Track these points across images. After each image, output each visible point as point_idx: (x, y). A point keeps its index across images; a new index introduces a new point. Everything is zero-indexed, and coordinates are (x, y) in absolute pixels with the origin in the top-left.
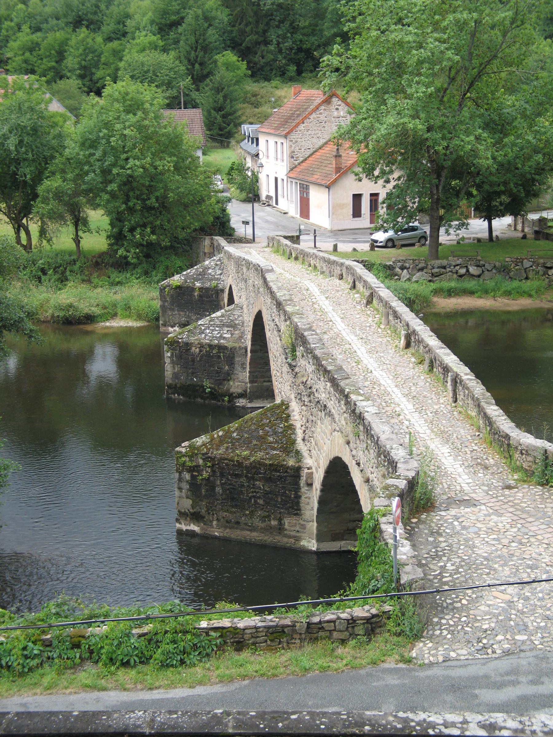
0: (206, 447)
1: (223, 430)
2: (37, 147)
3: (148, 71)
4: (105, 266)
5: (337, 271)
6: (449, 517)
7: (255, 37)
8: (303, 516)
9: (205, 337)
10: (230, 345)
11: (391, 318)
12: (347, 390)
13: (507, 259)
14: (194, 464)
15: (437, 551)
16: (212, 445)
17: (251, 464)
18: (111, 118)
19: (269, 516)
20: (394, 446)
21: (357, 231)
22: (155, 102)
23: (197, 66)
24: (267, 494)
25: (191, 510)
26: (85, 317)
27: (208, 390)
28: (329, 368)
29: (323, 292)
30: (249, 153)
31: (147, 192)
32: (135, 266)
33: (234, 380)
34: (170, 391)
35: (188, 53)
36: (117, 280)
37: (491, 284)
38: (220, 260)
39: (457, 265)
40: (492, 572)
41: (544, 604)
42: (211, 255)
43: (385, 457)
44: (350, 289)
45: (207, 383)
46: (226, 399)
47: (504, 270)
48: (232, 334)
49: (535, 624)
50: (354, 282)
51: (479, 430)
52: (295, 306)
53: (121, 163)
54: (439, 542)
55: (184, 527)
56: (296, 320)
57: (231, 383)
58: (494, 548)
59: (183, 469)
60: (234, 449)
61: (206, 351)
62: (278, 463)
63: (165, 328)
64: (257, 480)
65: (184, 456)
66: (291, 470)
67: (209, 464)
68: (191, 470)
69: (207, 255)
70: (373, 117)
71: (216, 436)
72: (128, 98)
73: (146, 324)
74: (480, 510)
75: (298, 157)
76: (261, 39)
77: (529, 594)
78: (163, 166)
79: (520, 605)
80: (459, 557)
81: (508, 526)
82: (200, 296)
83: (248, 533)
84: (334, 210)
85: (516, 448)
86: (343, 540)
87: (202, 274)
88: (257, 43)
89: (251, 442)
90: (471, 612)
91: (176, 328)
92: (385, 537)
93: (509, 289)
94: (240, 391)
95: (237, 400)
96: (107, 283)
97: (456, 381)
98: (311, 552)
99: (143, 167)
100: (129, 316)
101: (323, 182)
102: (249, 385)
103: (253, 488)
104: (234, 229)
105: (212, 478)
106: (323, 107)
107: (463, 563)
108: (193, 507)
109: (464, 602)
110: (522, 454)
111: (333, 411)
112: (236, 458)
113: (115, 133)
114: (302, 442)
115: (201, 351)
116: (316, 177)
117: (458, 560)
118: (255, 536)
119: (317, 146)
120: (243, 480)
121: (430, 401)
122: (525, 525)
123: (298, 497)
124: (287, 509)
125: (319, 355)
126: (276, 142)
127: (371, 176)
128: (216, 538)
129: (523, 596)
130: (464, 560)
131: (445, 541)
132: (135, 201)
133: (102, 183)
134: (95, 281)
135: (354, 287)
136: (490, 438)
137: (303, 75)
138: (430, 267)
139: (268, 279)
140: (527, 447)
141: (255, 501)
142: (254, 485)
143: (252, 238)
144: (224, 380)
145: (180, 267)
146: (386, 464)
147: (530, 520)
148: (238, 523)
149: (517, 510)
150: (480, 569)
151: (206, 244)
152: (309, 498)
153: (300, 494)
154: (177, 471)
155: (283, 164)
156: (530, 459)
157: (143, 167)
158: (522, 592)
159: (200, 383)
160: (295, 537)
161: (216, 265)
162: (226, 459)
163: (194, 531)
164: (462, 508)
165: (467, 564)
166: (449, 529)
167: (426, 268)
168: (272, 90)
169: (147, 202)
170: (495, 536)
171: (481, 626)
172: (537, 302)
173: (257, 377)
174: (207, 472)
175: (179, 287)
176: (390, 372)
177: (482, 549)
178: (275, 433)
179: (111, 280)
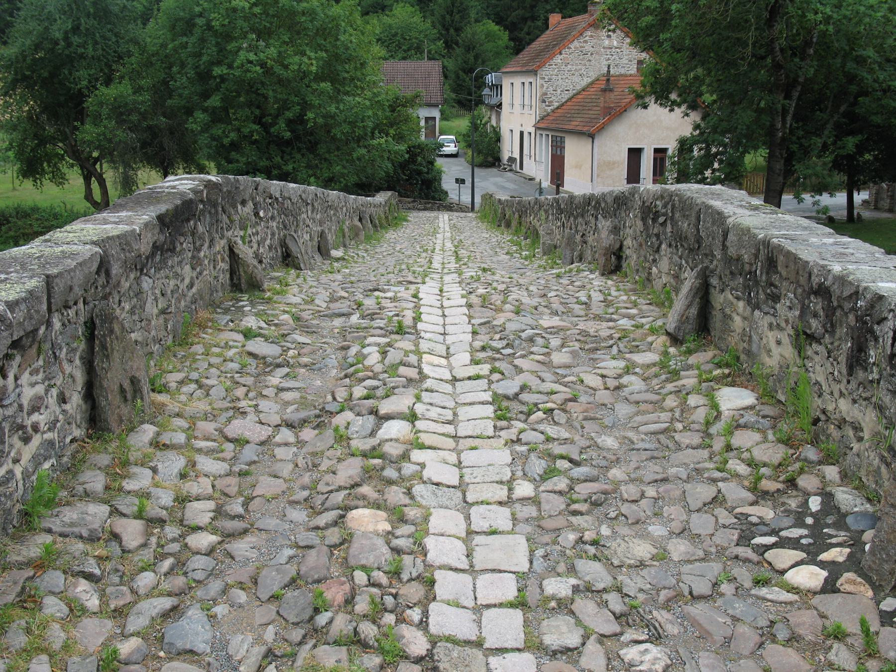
2: (104, 37)
3: (396, 35)
7: (520, 12)
23: (452, 31)
35: (443, 17)
44: (675, 339)
52: (183, 65)
75: (552, 102)
76: (528, 15)
88: (524, 20)
99: (263, 65)
106: (589, 33)
119: (579, 88)
155: (531, 112)
157: (263, 65)
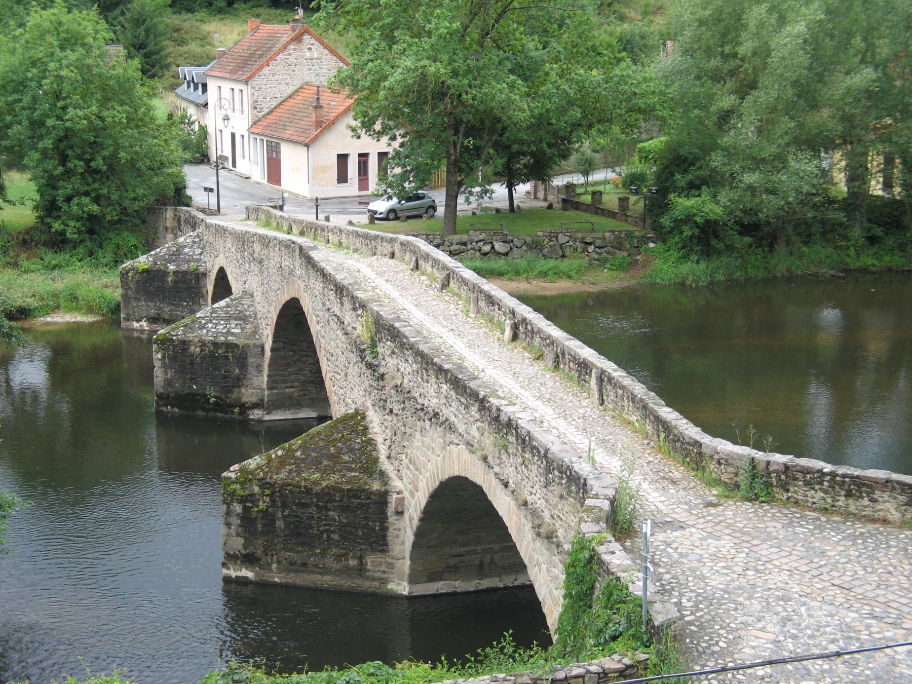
0: (263, 471)
1: (282, 449)
4: (36, 245)
5: (387, 248)
6: (659, 543)
8: (391, 553)
9: (207, 333)
10: (241, 342)
11: (482, 304)
12: (483, 393)
13: (540, 232)
14: (247, 492)
15: (662, 585)
16: (270, 467)
17: (323, 489)
18: (41, 55)
19: (346, 555)
20: (574, 459)
21: (348, 200)
22: (99, 36)
24: (344, 527)
25: (243, 552)
26: (18, 310)
27: (212, 400)
28: (446, 366)
29: (381, 274)
30: (192, 102)
31: (90, 150)
32: (75, 245)
33: (247, 386)
34: (161, 403)
36: (54, 262)
37: (522, 263)
38: (198, 236)
39: (480, 241)
40: (739, 607)
41: (817, 642)
42: (177, 230)
43: (561, 473)
45: (212, 392)
46: (236, 410)
47: (535, 246)
48: (242, 329)
49: (817, 667)
50: (417, 261)
51: (647, 436)
53: (59, 112)
54: (660, 573)
55: (233, 573)
56: (375, 308)
57: (243, 390)
58: (729, 578)
59: (232, 499)
60: (299, 472)
61: (210, 351)
62: (359, 487)
63: (128, 323)
64: (330, 510)
65: (233, 483)
66: (375, 495)
67: (267, 492)
68: (243, 500)
69: (170, 230)
70: (382, 58)
71: (273, 456)
72: (61, 29)
73: (99, 318)
74: (692, 534)
77: (795, 632)
78: (113, 117)
79: (790, 645)
80: (692, 591)
81: (733, 551)
82: (175, 282)
83: (319, 577)
84: (314, 174)
85: (712, 457)
86: (441, 580)
87: (176, 255)
89: (321, 463)
90: (736, 656)
91: (144, 324)
92: (613, 570)
93: (545, 270)
94: (254, 400)
95: (250, 412)
96: (40, 267)
97: (603, 379)
98: (401, 597)
100: (77, 309)
101: (301, 139)
102: (266, 392)
103: (325, 520)
104: (190, 198)
105: (270, 510)
106: (292, 47)
107: (700, 598)
108: (245, 546)
109: (721, 644)
110: (719, 463)
111: (453, 419)
112: (303, 483)
113: (47, 73)
114: (386, 461)
115: (202, 351)
116: (287, 134)
117: (693, 594)
118: (328, 581)
119: (285, 95)
120: (313, 510)
121: (570, 404)
122: (754, 549)
123: (384, 529)
124: (370, 544)
125: (426, 351)
126: (233, 89)
127: (372, 133)
128: (276, 585)
129: (788, 634)
130: (699, 595)
131: (667, 573)
132: (76, 162)
133: (30, 138)
134: (25, 264)
135: (417, 267)
136: (666, 447)
137: (235, 6)
138: (447, 243)
139: (316, 259)
140: (727, 455)
141: (328, 537)
142: (326, 516)
143: (216, 208)
144: (233, 387)
145: (135, 245)
146: (564, 482)
147: (755, 542)
148: (305, 565)
149: (735, 531)
150: (724, 604)
151: (168, 216)
152: (399, 530)
153: (386, 525)
154: (224, 502)
156: (730, 469)
158: (786, 629)
159: (201, 392)
160: (380, 579)
161: (194, 242)
162: (290, 485)
163: (246, 578)
164: (669, 531)
165: (706, 598)
166: (665, 557)
167: (443, 244)
168: (197, 24)
169: (92, 164)
170: (723, 564)
171: (755, 673)
172: (579, 284)
173: (277, 382)
174: (264, 502)
175: (147, 271)
176: (505, 370)
177: (714, 580)
178: (351, 450)
179: (46, 264)
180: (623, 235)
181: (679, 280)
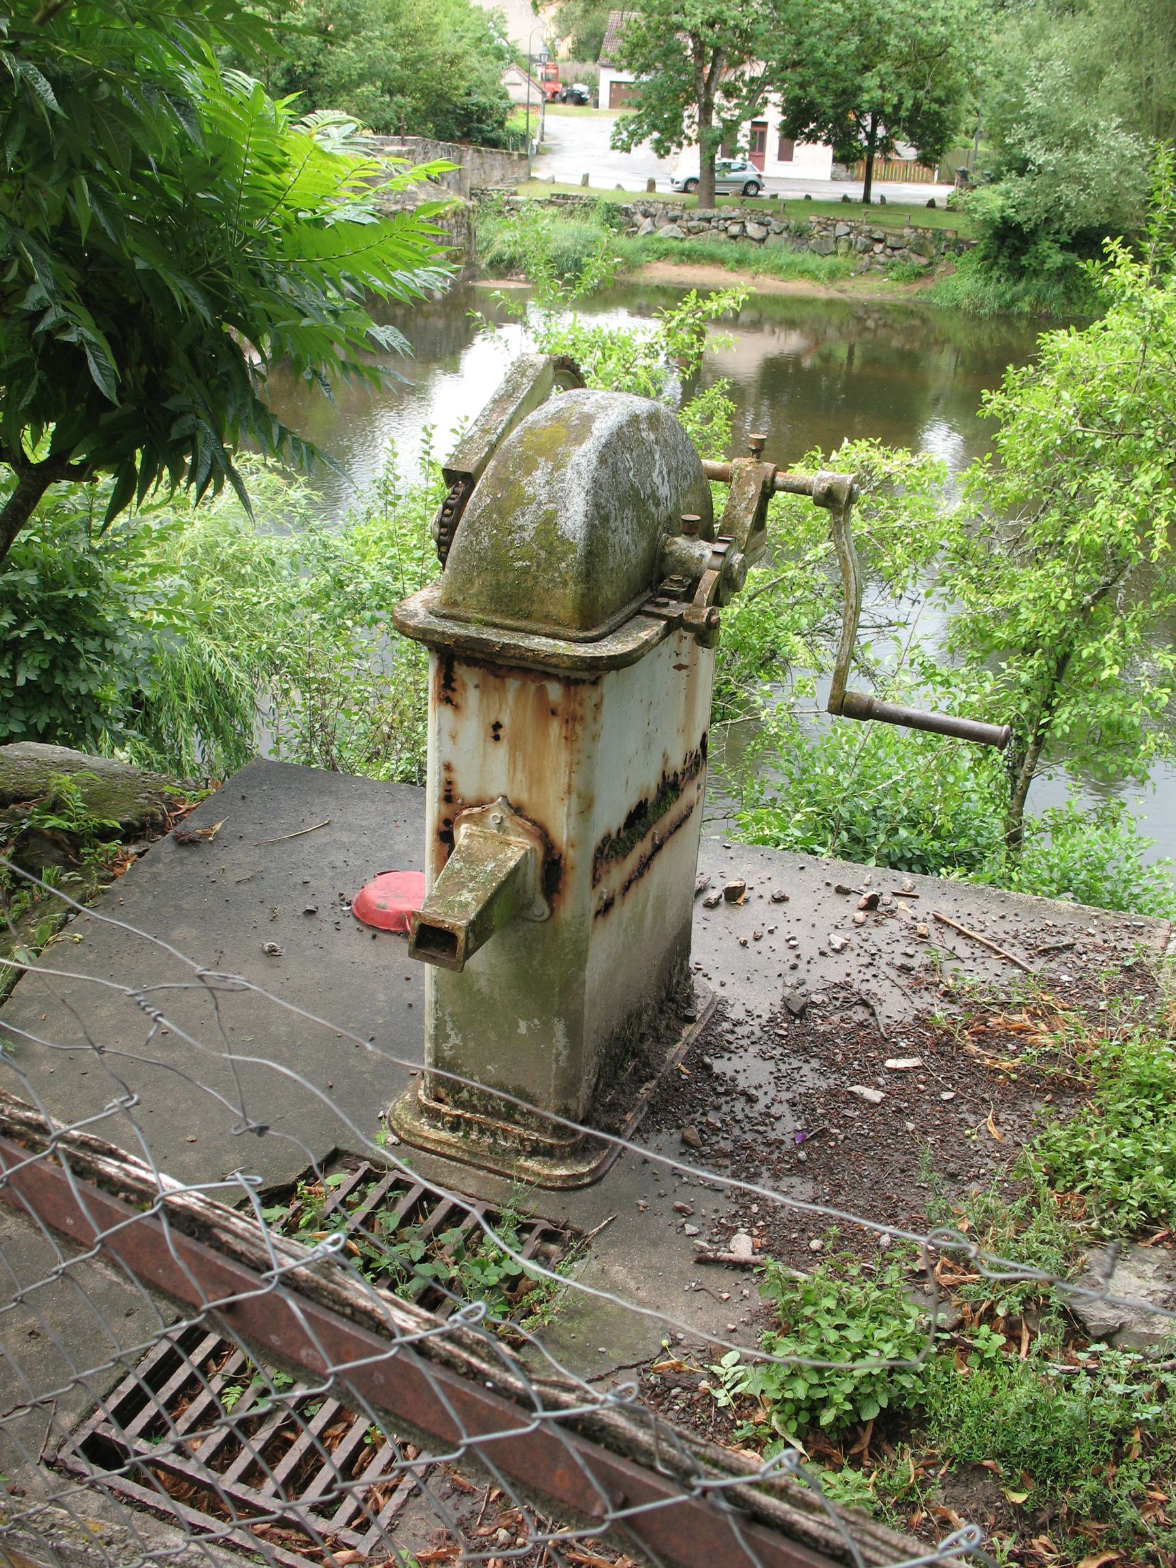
180: (929, 235)
181: (203, 151)
